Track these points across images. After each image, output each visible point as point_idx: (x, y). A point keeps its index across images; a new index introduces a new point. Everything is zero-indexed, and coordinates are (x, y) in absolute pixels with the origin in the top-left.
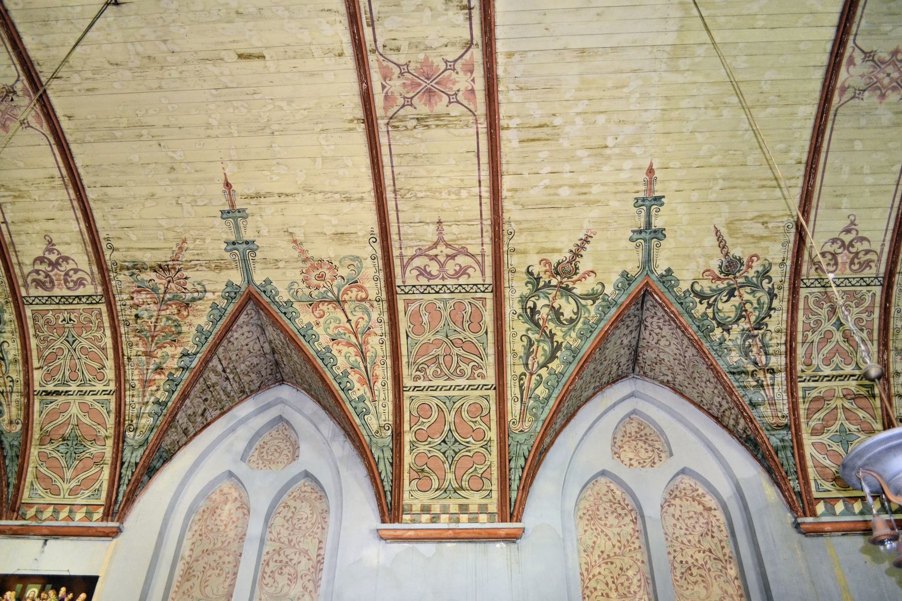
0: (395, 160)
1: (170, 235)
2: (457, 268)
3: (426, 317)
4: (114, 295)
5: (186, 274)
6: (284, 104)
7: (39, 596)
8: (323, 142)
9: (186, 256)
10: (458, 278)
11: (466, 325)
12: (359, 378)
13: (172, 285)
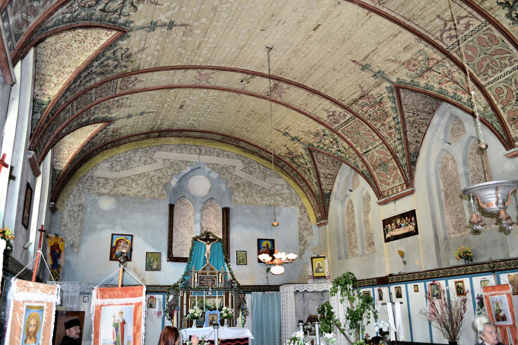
0: (396, 11)
1: (354, 86)
2: (464, 25)
3: (469, 52)
4: (357, 113)
5: (371, 93)
6: (341, 29)
7: (401, 222)
8: (366, 27)
9: (365, 89)
10: (468, 29)
11: (490, 44)
12: (462, 92)
13: (370, 100)
